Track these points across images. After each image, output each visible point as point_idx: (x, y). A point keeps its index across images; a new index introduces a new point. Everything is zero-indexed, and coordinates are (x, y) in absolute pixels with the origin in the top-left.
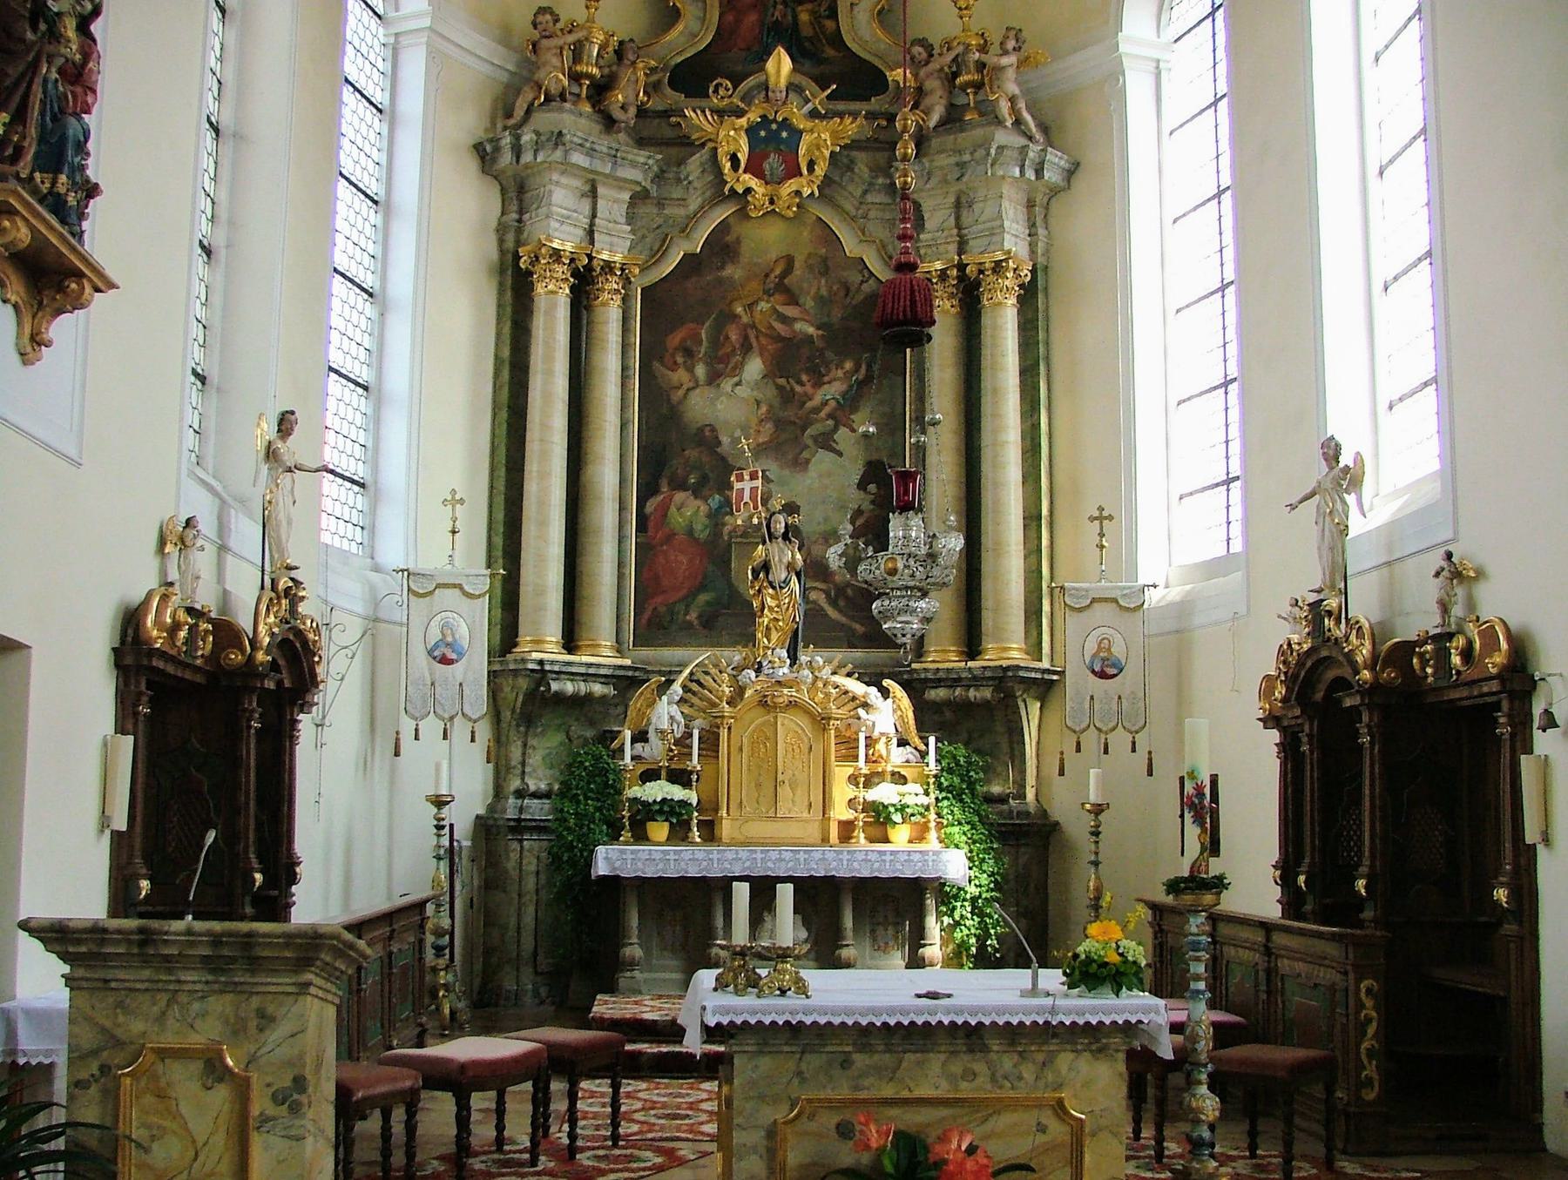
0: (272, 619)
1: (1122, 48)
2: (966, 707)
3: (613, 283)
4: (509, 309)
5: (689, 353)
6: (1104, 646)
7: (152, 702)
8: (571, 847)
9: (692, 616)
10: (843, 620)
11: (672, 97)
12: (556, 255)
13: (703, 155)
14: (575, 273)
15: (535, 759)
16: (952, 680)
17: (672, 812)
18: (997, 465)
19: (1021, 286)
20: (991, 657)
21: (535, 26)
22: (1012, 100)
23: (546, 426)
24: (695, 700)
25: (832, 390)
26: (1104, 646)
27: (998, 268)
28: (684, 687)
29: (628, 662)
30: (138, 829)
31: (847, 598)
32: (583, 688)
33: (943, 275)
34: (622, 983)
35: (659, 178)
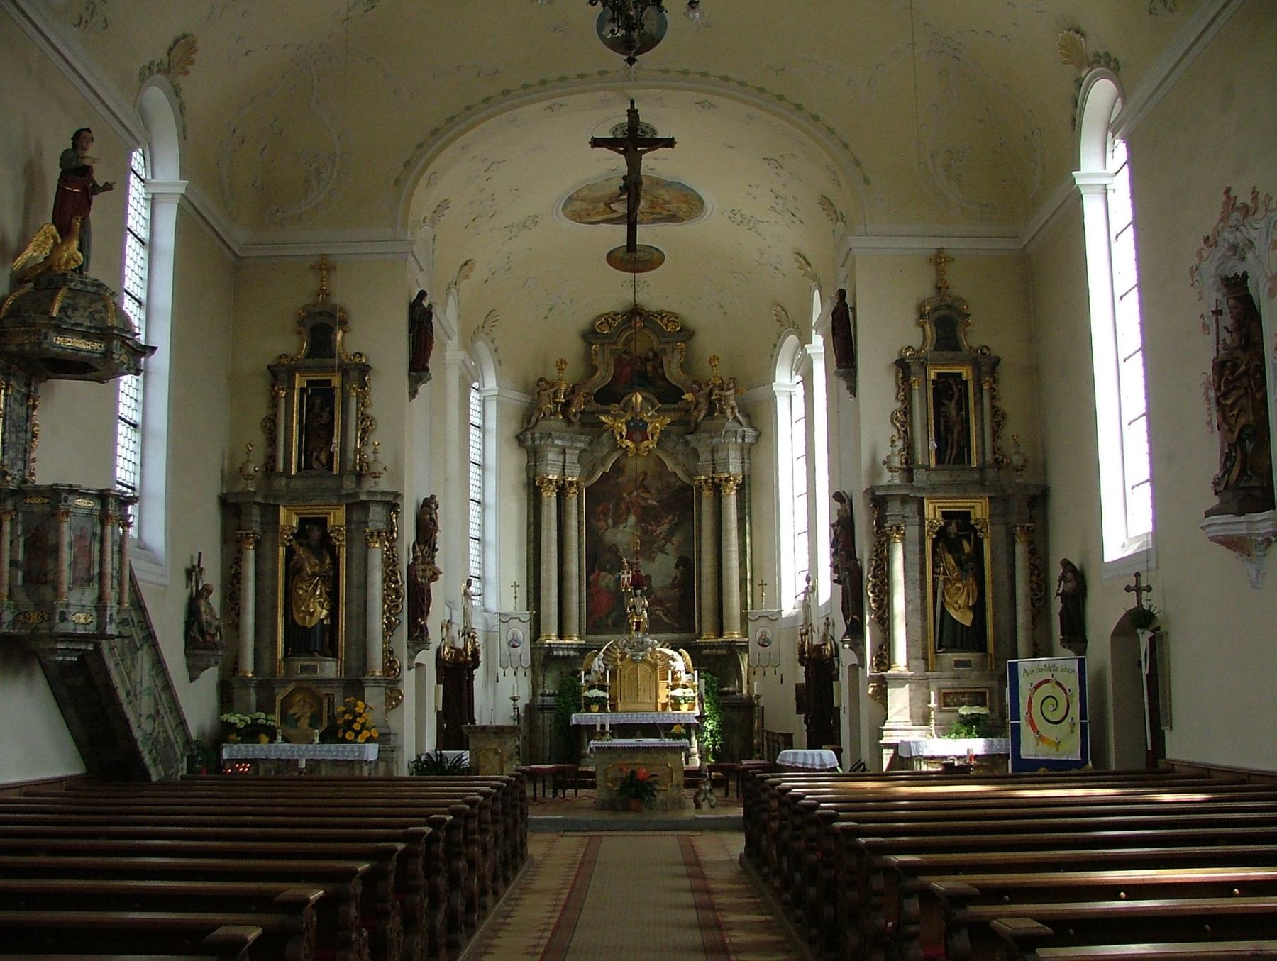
1: (774, 389)
2: (717, 657)
4: (532, 503)
5: (605, 514)
6: (764, 634)
8: (563, 715)
9: (610, 622)
10: (670, 622)
13: (609, 432)
14: (558, 487)
15: (548, 682)
16: (712, 646)
17: (598, 700)
18: (729, 560)
20: (726, 638)
22: (733, 408)
23: (549, 551)
25: (664, 528)
26: (764, 634)
27: (727, 480)
29: (584, 642)
33: (706, 481)
34: (582, 763)
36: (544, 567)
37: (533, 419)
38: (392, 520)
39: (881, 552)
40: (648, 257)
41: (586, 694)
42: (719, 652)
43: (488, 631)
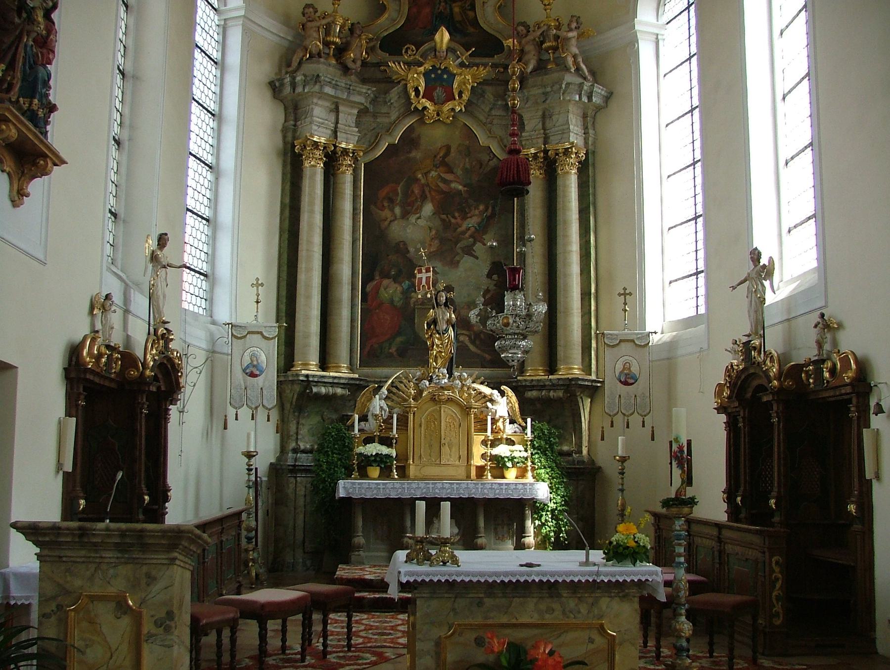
0: (154, 352)
1: (637, 27)
2: (548, 401)
5: (391, 201)
6: (627, 366)
7: (86, 399)
9: (393, 350)
11: (382, 55)
12: (316, 145)
14: (326, 155)
15: (304, 431)
17: (381, 460)
18: (566, 264)
20: (562, 373)
21: (304, 14)
22: (575, 57)
23: (310, 242)
25: (472, 222)
26: (627, 366)
27: (567, 152)
28: (388, 390)
29: (357, 376)
30: (79, 471)
33: (535, 156)
34: (353, 558)
36: (302, 265)
41: (361, 449)
42: (552, 394)
43: (214, 352)
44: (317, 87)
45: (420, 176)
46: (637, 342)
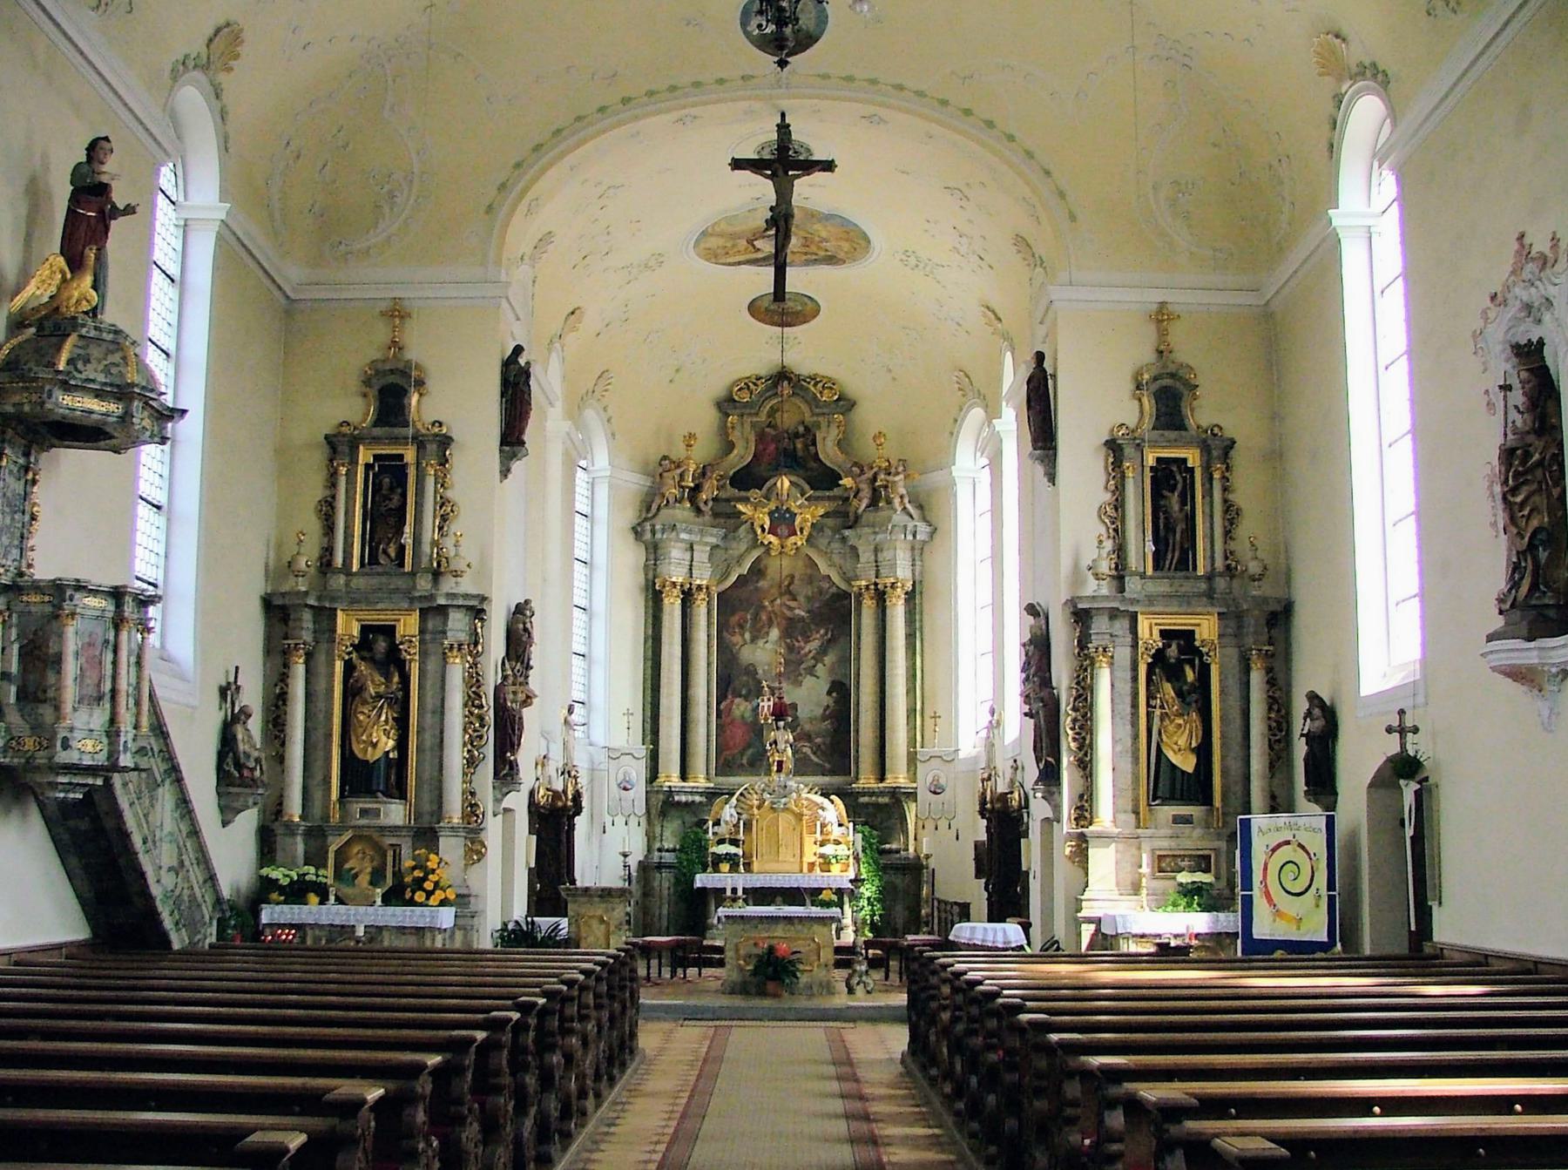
2: (877, 806)
3: (702, 595)
5: (741, 627)
6: (936, 779)
8: (685, 875)
9: (745, 761)
11: (731, 492)
12: (674, 584)
14: (683, 592)
15: (667, 833)
16: (872, 794)
17: (730, 858)
19: (906, 593)
20: (889, 782)
21: (661, 465)
22: (902, 497)
24: (743, 806)
25: (814, 645)
26: (936, 779)
28: (738, 800)
29: (712, 785)
31: (821, 751)
32: (690, 798)
33: (867, 587)
34: (708, 935)
35: (725, 537)
37: (654, 507)
38: (476, 629)
39: (1083, 679)
40: (799, 308)
41: (712, 850)
43: (593, 770)
44: (674, 533)
45: (767, 603)
46: (945, 758)
